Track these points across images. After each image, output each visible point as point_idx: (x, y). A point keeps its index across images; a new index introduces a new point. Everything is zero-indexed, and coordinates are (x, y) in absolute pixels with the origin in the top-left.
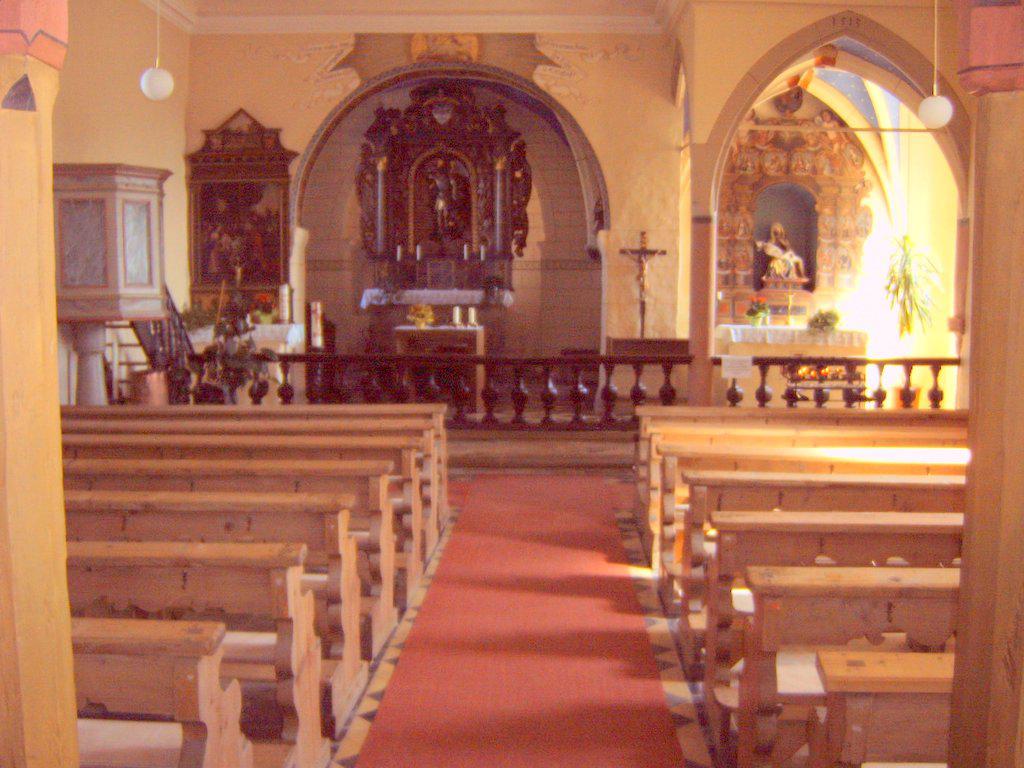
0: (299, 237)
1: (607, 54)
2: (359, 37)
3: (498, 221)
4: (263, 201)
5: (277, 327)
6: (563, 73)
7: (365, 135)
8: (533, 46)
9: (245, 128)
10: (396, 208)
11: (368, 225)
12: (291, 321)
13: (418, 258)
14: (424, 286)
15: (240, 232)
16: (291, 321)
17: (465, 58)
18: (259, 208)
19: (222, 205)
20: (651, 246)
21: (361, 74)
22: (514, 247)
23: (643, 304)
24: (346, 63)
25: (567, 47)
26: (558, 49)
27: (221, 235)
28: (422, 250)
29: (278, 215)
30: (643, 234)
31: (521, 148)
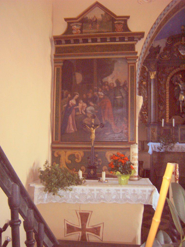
4: (114, 73)
9: (99, 17)
10: (160, 100)
13: (174, 125)
15: (94, 99)
18: (110, 80)
19: (79, 77)
27: (77, 101)
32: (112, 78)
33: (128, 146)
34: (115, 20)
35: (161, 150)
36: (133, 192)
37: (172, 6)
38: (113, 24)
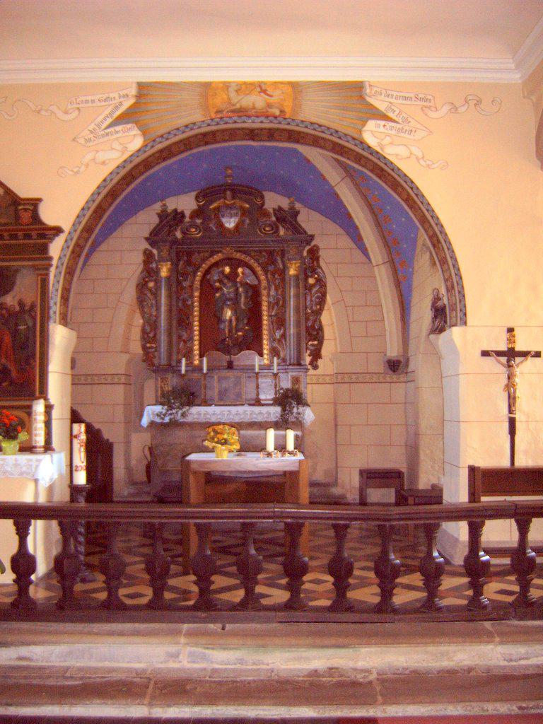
0: (60, 338)
1: (454, 109)
2: (142, 87)
3: (292, 330)
4: (16, 288)
5: (24, 458)
6: (400, 130)
7: (147, 239)
8: (362, 98)
10: (181, 319)
11: (149, 336)
12: (48, 447)
14: (206, 403)
16: (48, 447)
17: (277, 112)
20: (519, 347)
21: (144, 134)
22: (308, 359)
23: (512, 422)
24: (125, 118)
25: (406, 98)
26: (393, 100)
28: (208, 362)
29: (33, 307)
30: (510, 330)
31: (314, 253)
32: (13, 297)
33: (27, 403)
34: (20, 204)
35: (163, 419)
36: (14, 462)
37: (112, 180)
38: (16, 211)
